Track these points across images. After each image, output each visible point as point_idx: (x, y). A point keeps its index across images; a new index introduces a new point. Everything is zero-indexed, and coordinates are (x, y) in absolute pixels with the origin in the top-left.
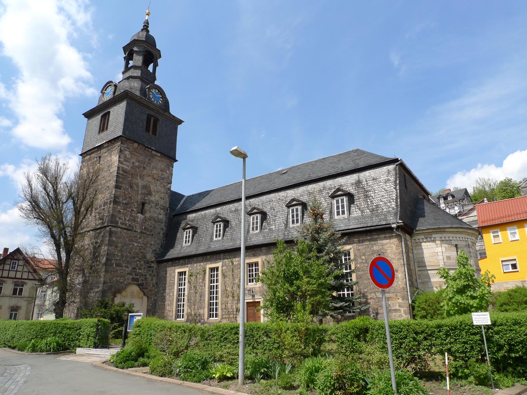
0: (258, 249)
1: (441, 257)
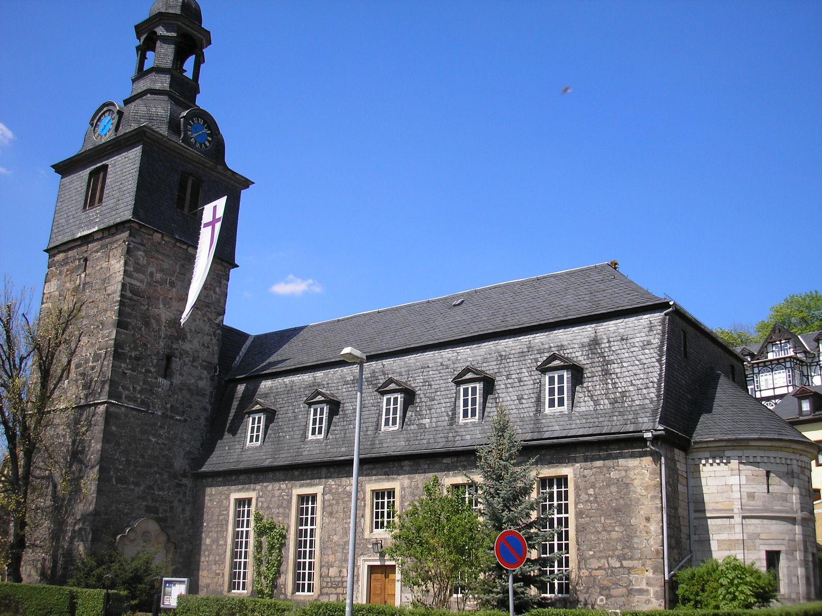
0: (396, 464)
1: (738, 495)
